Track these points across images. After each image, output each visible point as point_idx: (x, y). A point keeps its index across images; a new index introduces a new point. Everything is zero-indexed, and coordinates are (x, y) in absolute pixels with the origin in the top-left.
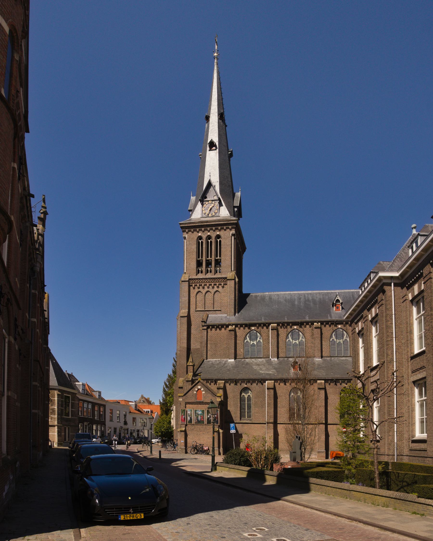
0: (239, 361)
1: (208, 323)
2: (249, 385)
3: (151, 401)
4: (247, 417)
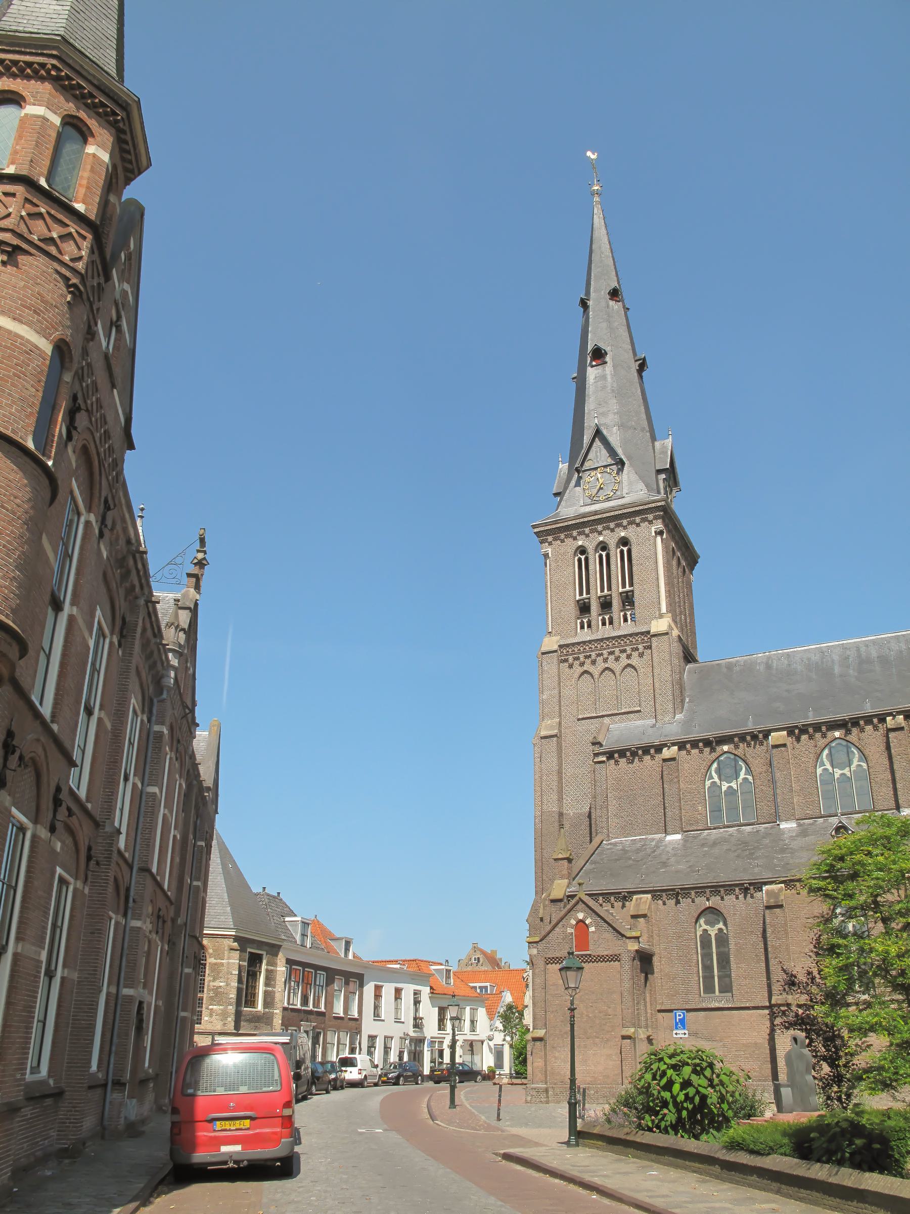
0: (695, 837)
1: (607, 745)
2: (715, 901)
3: (501, 960)
4: (720, 992)
